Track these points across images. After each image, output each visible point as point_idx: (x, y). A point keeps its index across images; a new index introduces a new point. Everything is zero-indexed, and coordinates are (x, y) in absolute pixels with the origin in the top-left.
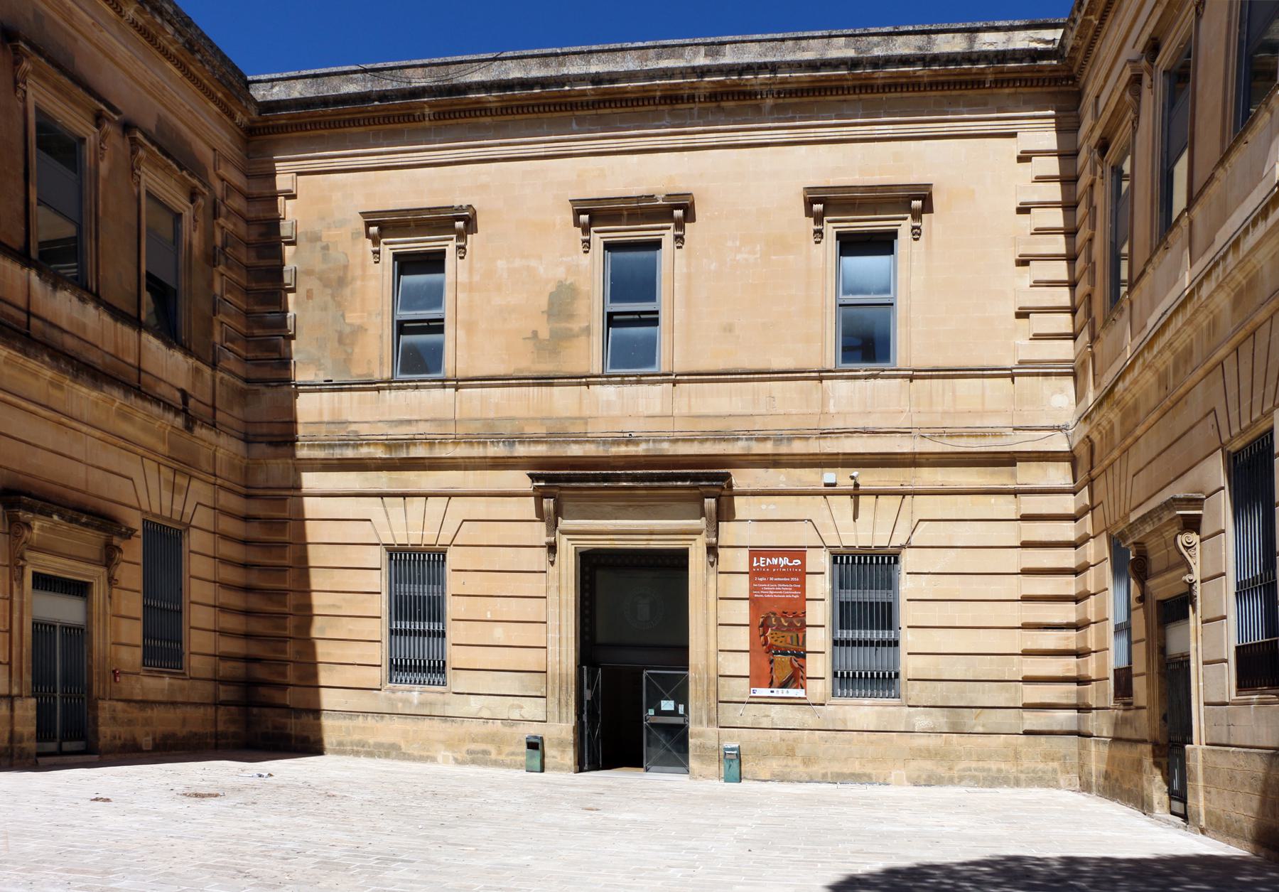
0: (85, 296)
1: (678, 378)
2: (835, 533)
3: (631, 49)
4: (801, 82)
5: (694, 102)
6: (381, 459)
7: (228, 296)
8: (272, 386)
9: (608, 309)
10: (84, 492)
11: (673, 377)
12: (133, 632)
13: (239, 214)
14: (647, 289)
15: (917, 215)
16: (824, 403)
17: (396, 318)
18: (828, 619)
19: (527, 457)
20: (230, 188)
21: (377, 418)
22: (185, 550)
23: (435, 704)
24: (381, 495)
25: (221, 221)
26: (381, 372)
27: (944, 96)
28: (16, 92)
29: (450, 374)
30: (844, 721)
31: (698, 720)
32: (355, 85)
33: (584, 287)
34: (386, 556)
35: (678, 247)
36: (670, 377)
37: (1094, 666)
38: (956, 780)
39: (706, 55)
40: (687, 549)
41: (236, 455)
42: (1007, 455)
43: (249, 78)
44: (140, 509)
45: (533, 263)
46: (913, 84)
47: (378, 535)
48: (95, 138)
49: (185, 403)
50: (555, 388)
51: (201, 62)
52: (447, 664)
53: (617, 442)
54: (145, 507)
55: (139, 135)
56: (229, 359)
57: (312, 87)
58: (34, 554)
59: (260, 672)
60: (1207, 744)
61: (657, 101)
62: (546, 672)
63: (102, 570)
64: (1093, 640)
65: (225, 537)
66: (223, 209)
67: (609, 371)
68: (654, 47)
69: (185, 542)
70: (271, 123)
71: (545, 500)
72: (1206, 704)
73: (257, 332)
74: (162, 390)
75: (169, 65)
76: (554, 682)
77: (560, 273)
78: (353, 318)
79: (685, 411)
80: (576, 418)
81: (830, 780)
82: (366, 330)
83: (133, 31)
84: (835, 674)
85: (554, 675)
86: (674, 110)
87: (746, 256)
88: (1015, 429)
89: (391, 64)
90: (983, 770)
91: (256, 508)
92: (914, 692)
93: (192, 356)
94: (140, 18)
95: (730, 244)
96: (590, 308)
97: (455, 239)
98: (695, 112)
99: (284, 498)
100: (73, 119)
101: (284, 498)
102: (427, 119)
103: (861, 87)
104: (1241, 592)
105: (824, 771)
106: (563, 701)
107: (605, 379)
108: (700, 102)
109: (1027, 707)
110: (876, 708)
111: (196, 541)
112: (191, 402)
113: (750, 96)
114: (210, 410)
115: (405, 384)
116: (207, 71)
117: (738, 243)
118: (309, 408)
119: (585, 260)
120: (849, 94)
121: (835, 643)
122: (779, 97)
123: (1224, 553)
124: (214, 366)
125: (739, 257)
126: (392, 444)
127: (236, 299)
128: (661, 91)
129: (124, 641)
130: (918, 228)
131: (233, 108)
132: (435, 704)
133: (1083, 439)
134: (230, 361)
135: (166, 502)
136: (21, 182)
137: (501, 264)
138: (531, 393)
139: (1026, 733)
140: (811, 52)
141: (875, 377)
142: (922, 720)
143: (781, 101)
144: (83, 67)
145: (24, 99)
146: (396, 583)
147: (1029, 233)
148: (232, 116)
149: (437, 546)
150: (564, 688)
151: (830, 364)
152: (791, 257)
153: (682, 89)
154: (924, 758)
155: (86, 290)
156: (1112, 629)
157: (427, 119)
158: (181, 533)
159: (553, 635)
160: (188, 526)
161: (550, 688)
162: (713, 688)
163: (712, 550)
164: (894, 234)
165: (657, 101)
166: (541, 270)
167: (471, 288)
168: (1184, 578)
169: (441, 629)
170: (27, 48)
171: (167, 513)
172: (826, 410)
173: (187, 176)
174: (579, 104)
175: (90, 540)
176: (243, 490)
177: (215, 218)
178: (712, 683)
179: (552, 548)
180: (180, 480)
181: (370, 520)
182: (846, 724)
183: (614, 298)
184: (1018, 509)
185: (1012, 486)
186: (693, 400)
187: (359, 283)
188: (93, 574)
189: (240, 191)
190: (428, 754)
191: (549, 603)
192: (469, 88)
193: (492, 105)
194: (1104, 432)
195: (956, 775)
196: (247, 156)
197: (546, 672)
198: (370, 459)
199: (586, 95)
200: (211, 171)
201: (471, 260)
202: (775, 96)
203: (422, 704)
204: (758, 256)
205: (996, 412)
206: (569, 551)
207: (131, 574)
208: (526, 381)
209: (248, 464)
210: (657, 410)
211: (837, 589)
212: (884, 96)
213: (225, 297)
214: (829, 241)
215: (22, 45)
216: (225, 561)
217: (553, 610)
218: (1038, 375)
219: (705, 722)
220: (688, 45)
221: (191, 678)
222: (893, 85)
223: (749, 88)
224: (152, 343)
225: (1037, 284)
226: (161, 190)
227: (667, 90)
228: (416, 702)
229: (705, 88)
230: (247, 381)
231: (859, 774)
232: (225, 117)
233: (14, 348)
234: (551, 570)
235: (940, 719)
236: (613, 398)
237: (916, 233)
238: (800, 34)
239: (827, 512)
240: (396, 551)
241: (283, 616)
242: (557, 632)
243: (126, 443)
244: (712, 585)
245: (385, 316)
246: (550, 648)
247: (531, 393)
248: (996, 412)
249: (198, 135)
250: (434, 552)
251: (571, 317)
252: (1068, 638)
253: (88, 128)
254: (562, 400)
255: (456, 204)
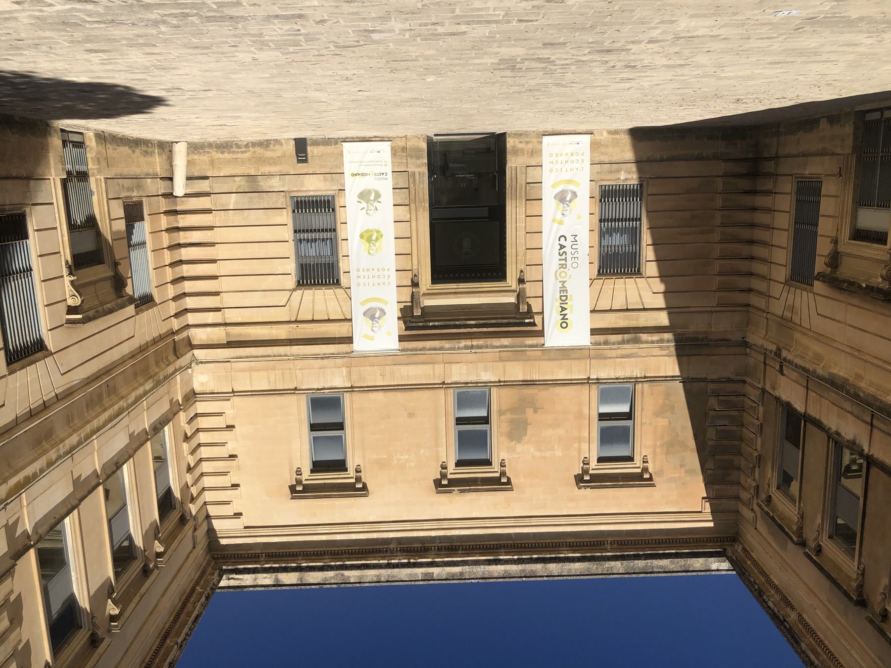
0: (836, 436)
1: (441, 386)
2: (338, 296)
3: (479, 579)
4: (373, 557)
5: (438, 547)
6: (644, 333)
7: (752, 437)
8: (725, 378)
9: (488, 426)
10: (849, 304)
11: (444, 386)
12: (827, 206)
13: (744, 489)
14: (464, 441)
15: (299, 482)
16: (349, 373)
17: (489, 425)
18: (340, 244)
19: (537, 336)
20: (748, 505)
21: (646, 359)
22: (789, 267)
23: (608, 172)
24: (644, 309)
25: (754, 484)
26: (642, 387)
27: (289, 549)
28: (864, 569)
29: (594, 387)
30: (325, 180)
31: (421, 175)
32: (659, 564)
33: (503, 439)
34: (642, 270)
35: (587, 458)
36: (446, 386)
37: (162, 222)
38: (250, 145)
39: (433, 574)
40: (433, 283)
41: (753, 333)
42: (233, 346)
43: (734, 573)
44: (814, 293)
45: (538, 454)
46: (308, 556)
47: (648, 283)
48: (822, 538)
49: (781, 367)
50: (521, 379)
51: (755, 583)
52: (598, 201)
53: (479, 347)
54: (811, 295)
55: (795, 539)
56: (754, 396)
57: (689, 565)
58: (883, 258)
59: (744, 184)
60: (49, 179)
61: (461, 547)
62: (527, 200)
63: (840, 250)
64: (164, 237)
65: (763, 277)
66: (752, 491)
67: (487, 389)
68: (465, 579)
69: (789, 272)
70: (719, 544)
71: (526, 311)
72: (52, 204)
73: (736, 413)
74: (794, 375)
75: (776, 582)
76: (521, 194)
77: (520, 448)
78: (663, 422)
79: (437, 366)
80: (507, 361)
81: (333, 140)
82: (653, 414)
83: (794, 604)
84: (333, 210)
85: (521, 198)
86: (451, 543)
87: (402, 457)
88: (229, 361)
89: (634, 576)
90: (234, 152)
91: (741, 298)
92: (281, 201)
93: (776, 397)
94: (788, 612)
95: (413, 465)
96: (499, 427)
97: (590, 469)
98: (438, 541)
99: (718, 305)
100: (833, 551)
101: (718, 305)
102: (609, 542)
103: (338, 554)
104: (28, 271)
105: (337, 146)
106: (514, 181)
107: (488, 384)
108: (435, 547)
109: (208, 194)
110: (305, 189)
111: (781, 274)
112: (778, 367)
113: (449, 548)
114: (767, 362)
115: (625, 380)
116: (753, 577)
117: (408, 464)
118: (670, 366)
119: (503, 455)
120: (345, 550)
121: (335, 230)
122: (387, 548)
123: (44, 293)
124: (764, 391)
125: (406, 457)
126: (637, 341)
127: (747, 433)
128: (458, 554)
129: (832, 199)
130: (297, 475)
131: (742, 555)
132: (608, 172)
133: (182, 356)
134: (754, 394)
135: (798, 299)
136: (868, 511)
137: (559, 453)
138: (537, 376)
139: (206, 178)
140: (371, 574)
141: (318, 389)
142: (275, 183)
143: (385, 547)
144: (826, 583)
145: (859, 564)
146: (636, 252)
147: (231, 473)
148: (744, 549)
149: (604, 278)
150: (514, 190)
151: (347, 396)
152: (375, 457)
153: (445, 554)
154: (272, 158)
155: (837, 443)
156: (148, 245)
157: (609, 542)
158: (791, 278)
159: (521, 225)
160: (786, 283)
161: (524, 189)
162: (412, 196)
163: (415, 284)
164: (312, 471)
165: (461, 547)
166: (532, 450)
167: (579, 440)
168: (75, 278)
169: (602, 224)
170: (852, 595)
171: (798, 291)
172: (348, 369)
173: (771, 513)
174: (509, 547)
175: (847, 270)
176: (751, 309)
177: (758, 486)
178: (413, 200)
179: (521, 281)
180: (788, 314)
181: (653, 293)
182: (324, 177)
183: (626, 429)
184: (223, 314)
185: (229, 328)
186: (432, 373)
187: (658, 443)
188: (847, 246)
189: (744, 504)
190: (613, 136)
191: (524, 245)
192: (579, 560)
193: (566, 549)
194: (165, 361)
195: (251, 148)
196: (738, 525)
197: (527, 200)
198: (652, 333)
199: (505, 552)
200: (759, 516)
201: (579, 456)
202: (388, 549)
203: (618, 171)
204: (395, 458)
205: (242, 371)
206: (510, 280)
207: (823, 248)
208: (541, 383)
209: (747, 327)
210: (454, 367)
211: (335, 263)
212: (324, 549)
213: (755, 436)
214: (351, 466)
215: (855, 598)
216: (764, 261)
217: (521, 241)
218: (218, 393)
219: (417, 174)
220: (444, 580)
221: (792, 175)
222: (255, 558)
223: (405, 554)
224: (799, 407)
225: (223, 444)
226: (788, 505)
227: (455, 554)
228: (623, 172)
229: (431, 555)
230: (744, 382)
231: (314, 145)
232: (748, 548)
233: (881, 401)
234: (522, 267)
235: (264, 184)
236: (483, 373)
237: (299, 472)
238: (377, 584)
239: (343, 309)
240: (635, 274)
241: (723, 225)
242: (518, 227)
243: (820, 338)
244: (415, 262)
245: (639, 422)
246: (523, 216)
247: (537, 376)
248: (242, 371)
249: (764, 538)
250: (607, 274)
251: (511, 422)
252: (186, 238)
253: (826, 545)
254: (516, 372)
255: (588, 490)
